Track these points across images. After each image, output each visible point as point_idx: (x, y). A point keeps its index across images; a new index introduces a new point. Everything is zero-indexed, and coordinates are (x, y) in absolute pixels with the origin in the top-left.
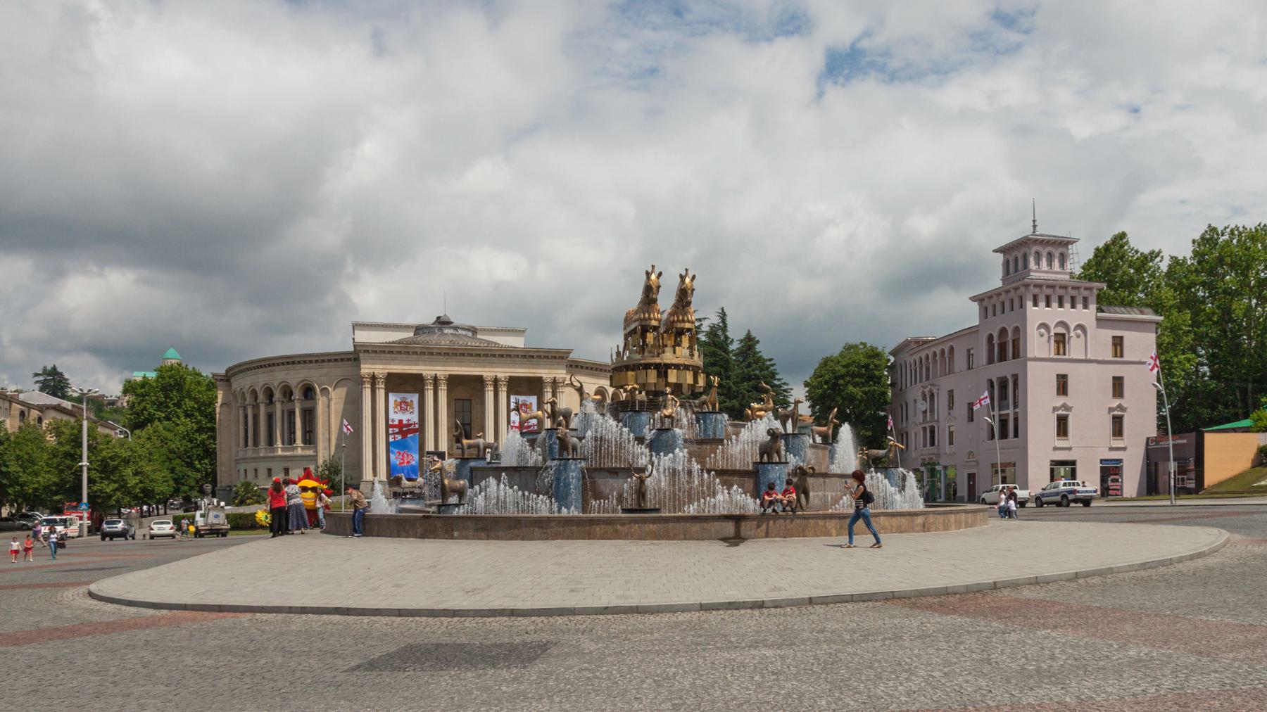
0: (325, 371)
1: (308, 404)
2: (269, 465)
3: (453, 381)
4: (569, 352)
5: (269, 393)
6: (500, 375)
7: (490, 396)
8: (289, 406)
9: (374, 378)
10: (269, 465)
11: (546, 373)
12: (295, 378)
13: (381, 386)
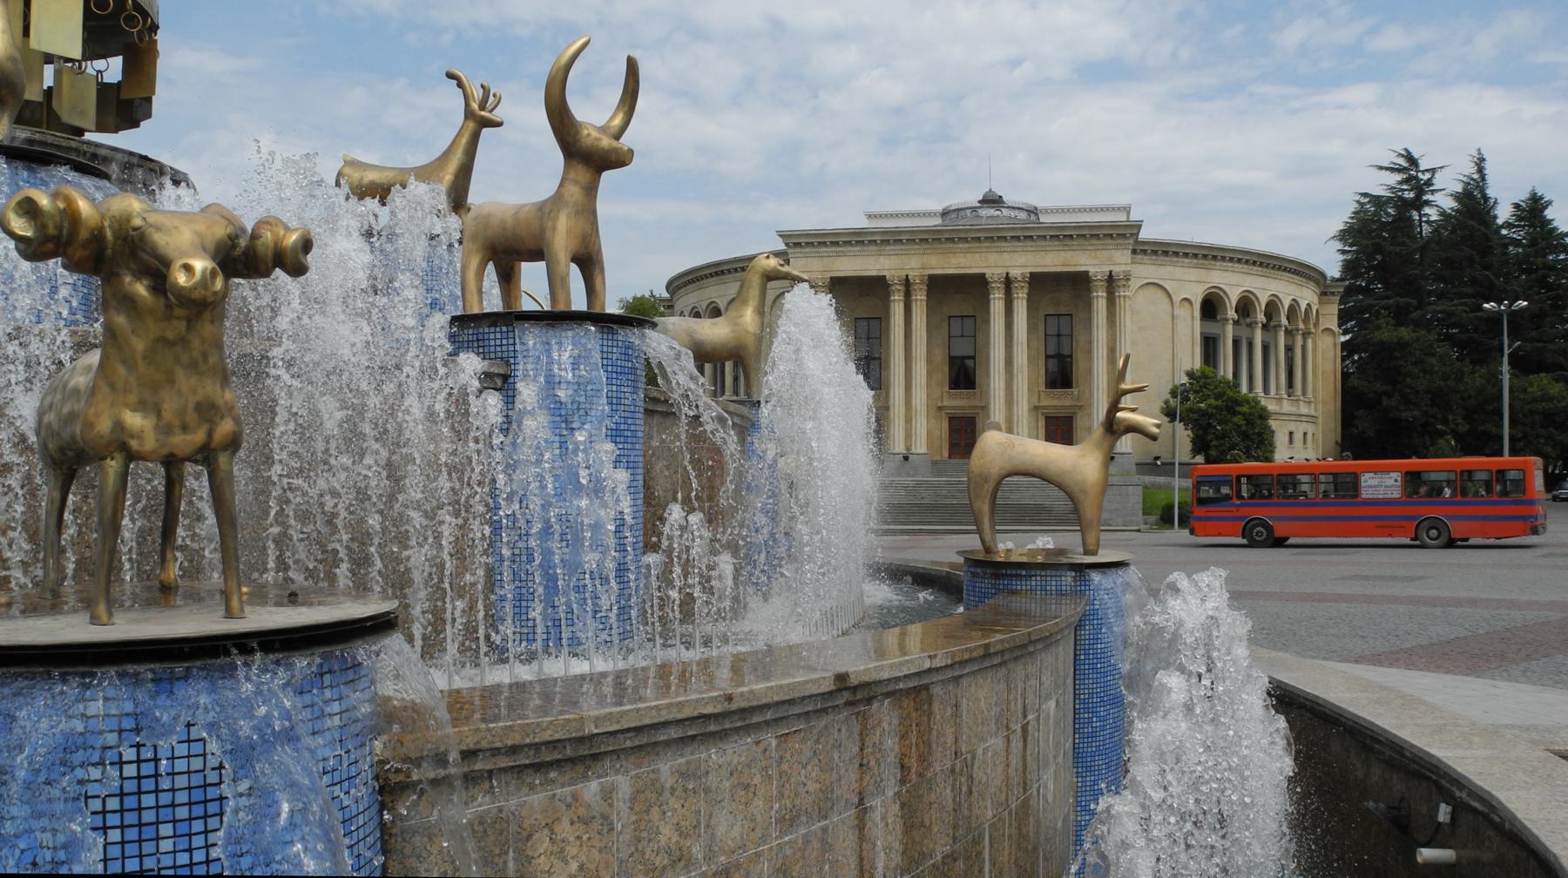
1: (1213, 328)
3: (1040, 283)
6: (1015, 273)
8: (1244, 333)
9: (1008, 282)
10: (1292, 427)
13: (920, 297)
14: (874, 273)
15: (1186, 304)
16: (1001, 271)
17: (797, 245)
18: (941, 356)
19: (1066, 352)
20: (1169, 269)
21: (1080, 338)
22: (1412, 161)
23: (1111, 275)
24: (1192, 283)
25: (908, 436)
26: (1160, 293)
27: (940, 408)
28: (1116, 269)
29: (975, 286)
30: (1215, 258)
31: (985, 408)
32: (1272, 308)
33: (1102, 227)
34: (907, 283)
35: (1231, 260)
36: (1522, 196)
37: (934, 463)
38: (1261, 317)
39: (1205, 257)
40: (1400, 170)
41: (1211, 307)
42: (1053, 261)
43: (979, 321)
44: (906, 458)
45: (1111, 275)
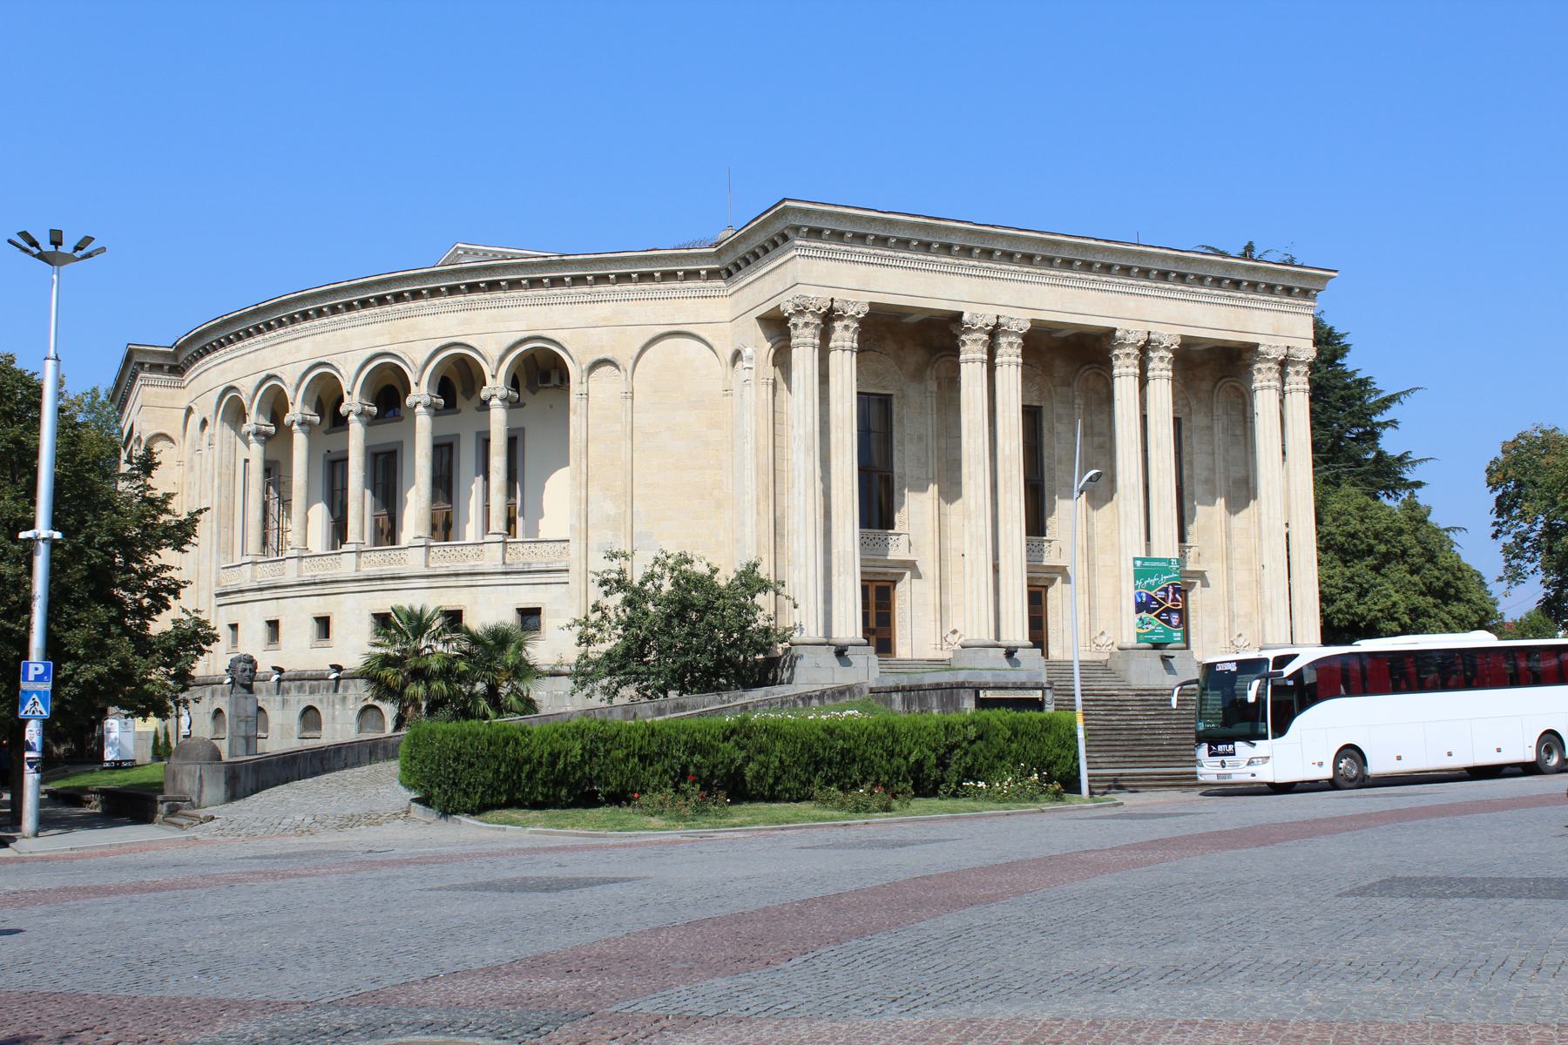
2: (271, 610)
5: (326, 395)
8: (331, 442)
10: (271, 610)
12: (492, 330)
13: (844, 336)
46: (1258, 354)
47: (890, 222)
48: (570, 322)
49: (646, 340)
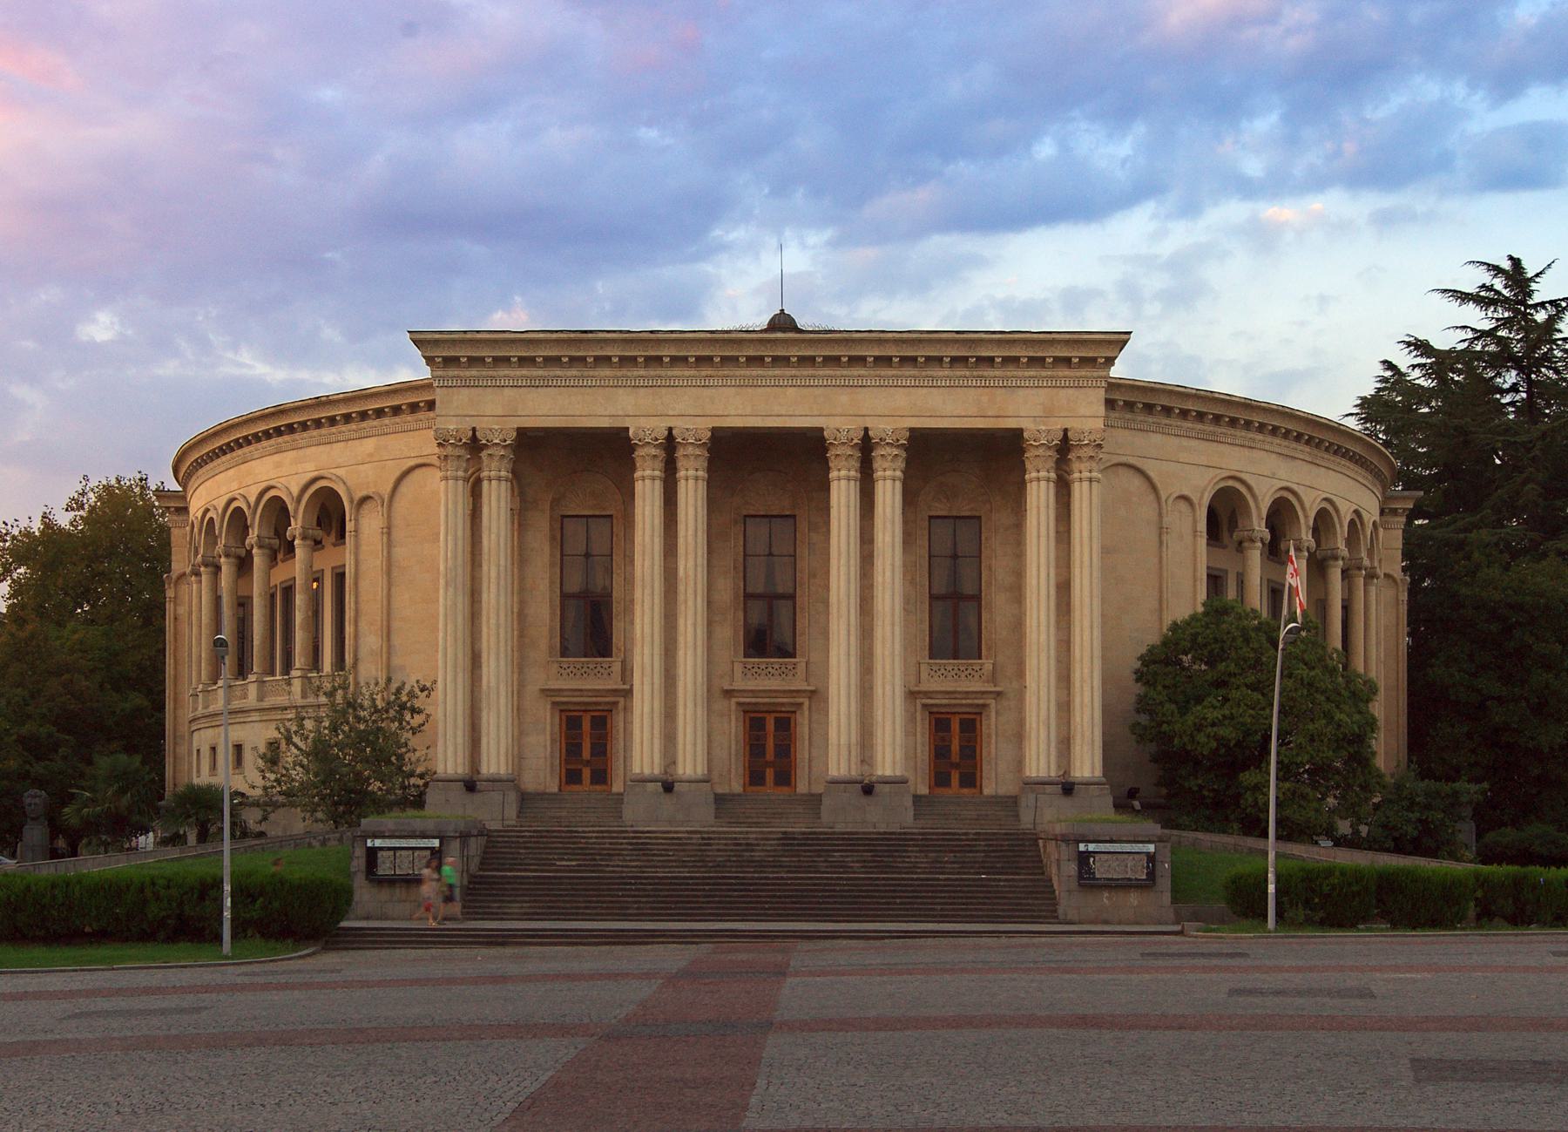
0: (369, 445)
3: (930, 452)
4: (1119, 341)
6: (881, 427)
7: (843, 493)
9: (866, 446)
11: (1024, 407)
13: (495, 469)
14: (605, 423)
15: (1183, 506)
16: (659, 427)
17: (450, 361)
18: (727, 589)
19: (968, 589)
20: (1156, 438)
21: (997, 564)
22: (1516, 275)
23: (866, 438)
24: (1194, 467)
25: (669, 738)
26: (1136, 482)
27: (728, 693)
28: (679, 425)
29: (608, 451)
30: (1233, 422)
31: (817, 695)
32: (1281, 513)
33: (1052, 342)
34: (670, 444)
35: (1261, 428)
36: (1381, 366)
37: (720, 799)
38: (1259, 527)
39: (1217, 419)
40: (1484, 299)
41: (1223, 515)
42: (953, 406)
43: (803, 526)
44: (668, 787)
45: (866, 438)
46: (823, 439)
47: (531, 341)
48: (350, 462)
49: (398, 474)
